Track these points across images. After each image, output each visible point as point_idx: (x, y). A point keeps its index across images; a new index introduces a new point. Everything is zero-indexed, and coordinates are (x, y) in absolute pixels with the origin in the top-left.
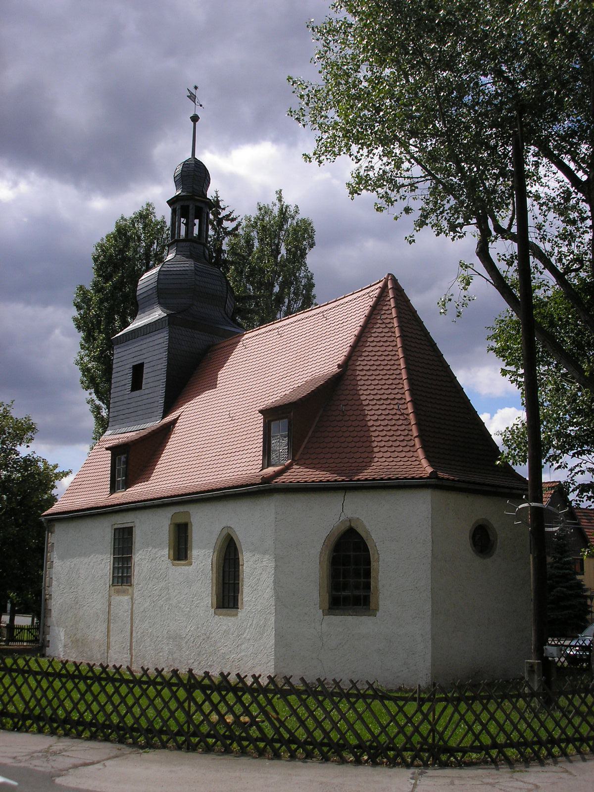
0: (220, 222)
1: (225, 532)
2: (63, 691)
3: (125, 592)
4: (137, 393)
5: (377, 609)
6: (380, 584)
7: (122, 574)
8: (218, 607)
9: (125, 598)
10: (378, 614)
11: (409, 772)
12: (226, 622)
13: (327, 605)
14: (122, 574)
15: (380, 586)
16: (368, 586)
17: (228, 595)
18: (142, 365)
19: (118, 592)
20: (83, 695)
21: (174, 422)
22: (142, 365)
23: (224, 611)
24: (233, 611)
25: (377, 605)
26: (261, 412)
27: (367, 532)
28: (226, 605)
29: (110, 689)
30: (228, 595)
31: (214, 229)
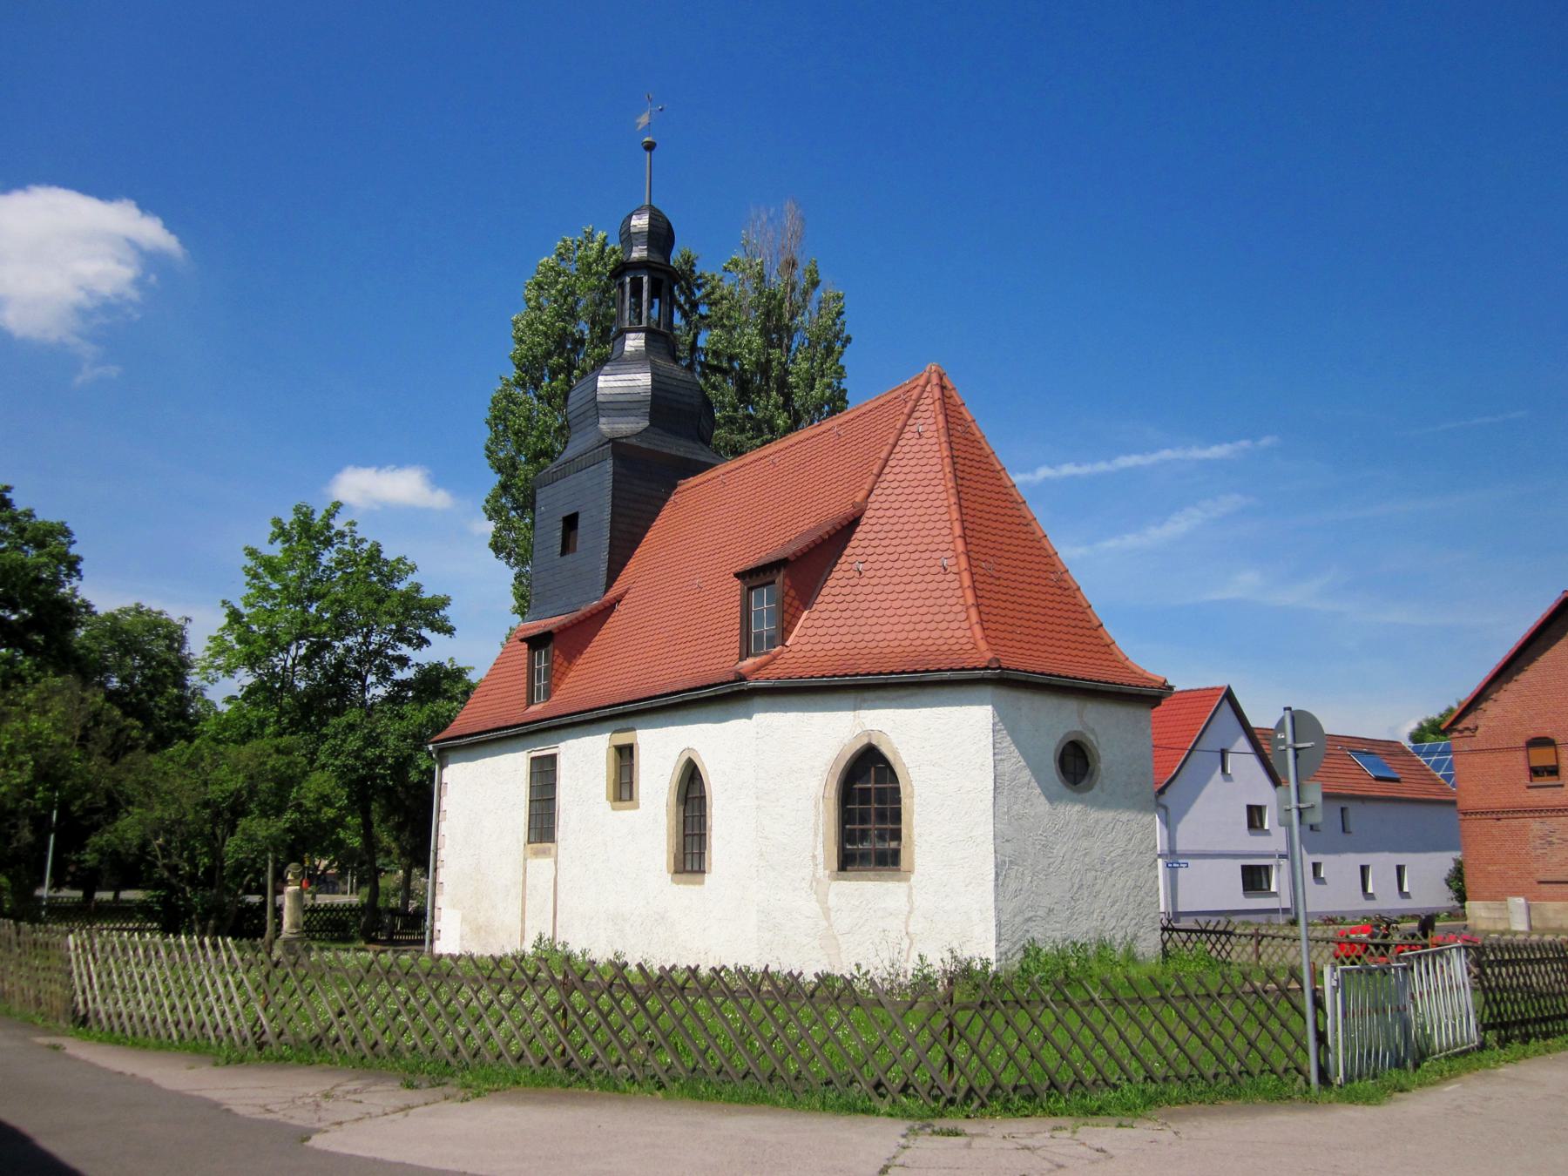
0: (695, 306)
1: (684, 759)
2: (1035, 1032)
3: (545, 853)
4: (568, 557)
5: (911, 871)
6: (916, 831)
7: (542, 822)
8: (676, 872)
9: (545, 863)
10: (913, 878)
11: (901, 1126)
12: (686, 893)
13: (835, 865)
14: (542, 822)
15: (915, 838)
16: (897, 835)
17: (690, 853)
18: (563, 553)
19: (536, 854)
20: (605, 1016)
21: (618, 600)
22: (563, 553)
23: (684, 877)
24: (698, 877)
25: (912, 864)
26: (737, 575)
27: (895, 753)
28: (688, 867)
29: (1238, 1011)
30: (690, 853)
31: (685, 315)
